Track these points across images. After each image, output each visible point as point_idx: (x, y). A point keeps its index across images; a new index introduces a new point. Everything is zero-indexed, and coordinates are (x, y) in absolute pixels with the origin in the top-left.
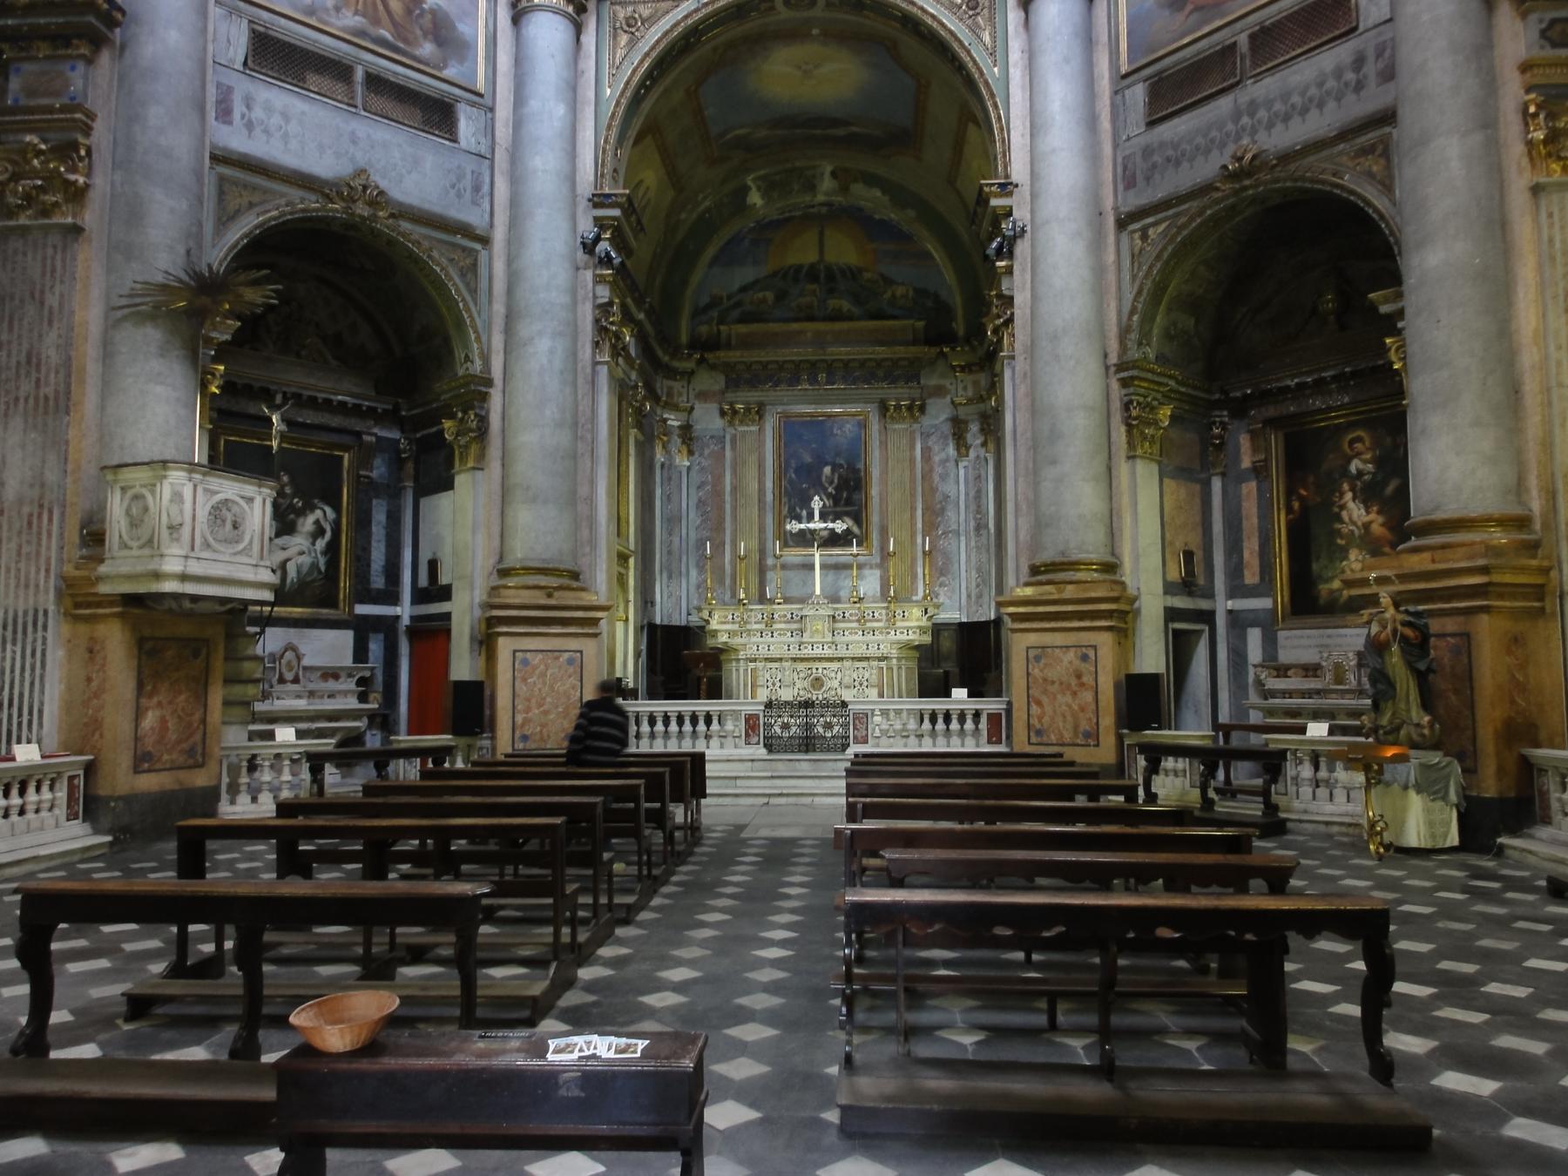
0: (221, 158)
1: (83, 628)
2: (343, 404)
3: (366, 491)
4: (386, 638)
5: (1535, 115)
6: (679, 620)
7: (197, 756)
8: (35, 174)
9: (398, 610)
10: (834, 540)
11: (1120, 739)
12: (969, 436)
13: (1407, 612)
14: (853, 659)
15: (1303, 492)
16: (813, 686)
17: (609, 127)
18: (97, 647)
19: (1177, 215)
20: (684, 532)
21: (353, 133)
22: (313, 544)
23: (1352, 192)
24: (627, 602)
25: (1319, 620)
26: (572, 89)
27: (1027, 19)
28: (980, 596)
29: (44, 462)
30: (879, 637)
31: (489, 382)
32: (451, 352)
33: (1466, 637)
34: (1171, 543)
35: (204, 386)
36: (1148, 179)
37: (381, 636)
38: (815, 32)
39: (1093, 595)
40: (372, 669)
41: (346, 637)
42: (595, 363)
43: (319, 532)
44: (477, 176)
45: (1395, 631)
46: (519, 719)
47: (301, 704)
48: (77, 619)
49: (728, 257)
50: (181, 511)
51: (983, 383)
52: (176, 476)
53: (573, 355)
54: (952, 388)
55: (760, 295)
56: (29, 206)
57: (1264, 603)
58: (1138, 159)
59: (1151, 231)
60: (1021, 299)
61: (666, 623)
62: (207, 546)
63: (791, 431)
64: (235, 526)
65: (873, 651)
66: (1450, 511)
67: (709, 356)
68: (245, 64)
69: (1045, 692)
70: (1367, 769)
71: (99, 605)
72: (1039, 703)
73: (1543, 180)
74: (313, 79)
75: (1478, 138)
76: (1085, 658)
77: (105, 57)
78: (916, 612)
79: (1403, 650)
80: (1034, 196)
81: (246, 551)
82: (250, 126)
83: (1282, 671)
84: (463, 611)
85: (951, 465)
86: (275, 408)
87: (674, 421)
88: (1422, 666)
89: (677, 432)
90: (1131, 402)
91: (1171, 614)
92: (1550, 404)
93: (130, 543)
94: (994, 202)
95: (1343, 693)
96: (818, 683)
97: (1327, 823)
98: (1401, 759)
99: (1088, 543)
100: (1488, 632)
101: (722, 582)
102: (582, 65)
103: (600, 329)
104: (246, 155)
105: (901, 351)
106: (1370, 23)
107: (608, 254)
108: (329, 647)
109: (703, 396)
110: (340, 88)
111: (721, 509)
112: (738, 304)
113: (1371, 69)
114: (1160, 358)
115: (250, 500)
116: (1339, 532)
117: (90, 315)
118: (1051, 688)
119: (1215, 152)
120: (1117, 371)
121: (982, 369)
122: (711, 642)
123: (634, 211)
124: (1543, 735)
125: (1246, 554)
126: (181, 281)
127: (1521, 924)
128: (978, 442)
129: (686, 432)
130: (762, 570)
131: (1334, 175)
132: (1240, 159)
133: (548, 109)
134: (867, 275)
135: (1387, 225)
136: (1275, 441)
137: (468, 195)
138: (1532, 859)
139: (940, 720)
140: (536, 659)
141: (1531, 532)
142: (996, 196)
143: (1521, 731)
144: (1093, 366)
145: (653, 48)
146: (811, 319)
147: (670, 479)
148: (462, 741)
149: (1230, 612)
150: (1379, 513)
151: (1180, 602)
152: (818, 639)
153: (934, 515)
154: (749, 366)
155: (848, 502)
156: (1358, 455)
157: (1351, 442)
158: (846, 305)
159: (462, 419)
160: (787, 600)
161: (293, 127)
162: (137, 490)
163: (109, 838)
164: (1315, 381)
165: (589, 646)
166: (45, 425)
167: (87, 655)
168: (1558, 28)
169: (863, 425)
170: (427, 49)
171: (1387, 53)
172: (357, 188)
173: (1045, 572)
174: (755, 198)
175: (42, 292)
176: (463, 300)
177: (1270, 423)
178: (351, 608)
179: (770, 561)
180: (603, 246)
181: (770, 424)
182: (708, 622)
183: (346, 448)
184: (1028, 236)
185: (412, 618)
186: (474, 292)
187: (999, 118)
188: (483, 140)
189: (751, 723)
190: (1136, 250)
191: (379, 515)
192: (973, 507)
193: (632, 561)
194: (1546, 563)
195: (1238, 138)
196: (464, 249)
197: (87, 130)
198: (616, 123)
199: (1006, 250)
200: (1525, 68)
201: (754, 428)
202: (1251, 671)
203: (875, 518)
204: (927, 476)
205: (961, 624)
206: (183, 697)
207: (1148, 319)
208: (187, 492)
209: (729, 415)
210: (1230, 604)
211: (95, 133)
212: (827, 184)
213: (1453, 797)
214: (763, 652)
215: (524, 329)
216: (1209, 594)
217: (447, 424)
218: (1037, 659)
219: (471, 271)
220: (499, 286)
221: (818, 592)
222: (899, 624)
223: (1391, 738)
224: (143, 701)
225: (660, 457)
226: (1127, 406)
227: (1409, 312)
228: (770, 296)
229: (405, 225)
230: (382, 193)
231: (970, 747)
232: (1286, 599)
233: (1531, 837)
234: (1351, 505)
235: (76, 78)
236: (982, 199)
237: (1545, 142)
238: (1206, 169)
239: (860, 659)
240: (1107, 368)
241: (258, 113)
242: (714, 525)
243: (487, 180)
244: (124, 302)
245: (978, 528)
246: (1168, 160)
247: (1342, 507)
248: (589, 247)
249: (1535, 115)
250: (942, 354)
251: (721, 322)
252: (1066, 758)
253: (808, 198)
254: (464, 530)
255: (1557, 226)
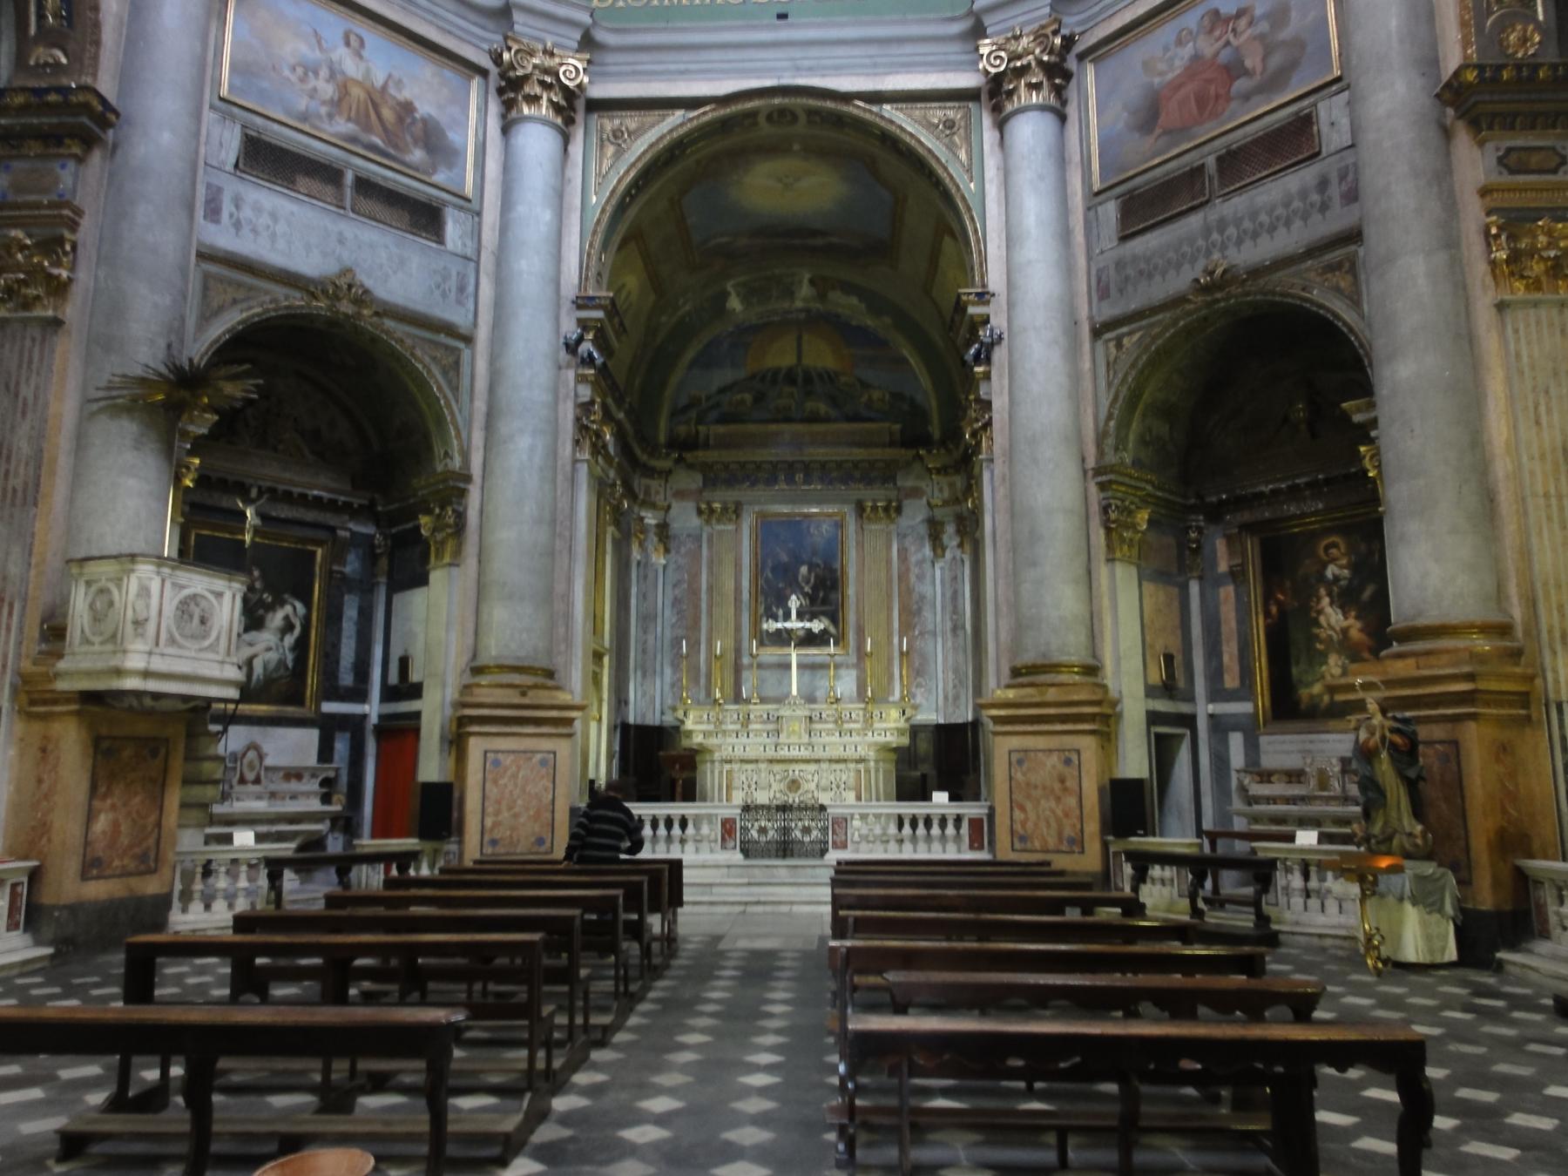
0: (207, 255)
1: (37, 727)
2: (318, 499)
3: (338, 586)
4: (353, 738)
5: (1497, 236)
6: (653, 719)
7: (149, 862)
8: (18, 268)
9: (366, 708)
10: (810, 639)
11: (1105, 846)
12: (945, 538)
13: (1394, 718)
14: (830, 761)
15: (1280, 597)
16: (790, 789)
17: (595, 232)
18: (50, 747)
19: (1152, 325)
20: (659, 629)
21: (340, 233)
22: (282, 640)
23: (1321, 306)
24: (600, 701)
25: (1303, 725)
26: (559, 196)
27: (1002, 137)
28: (956, 698)
29: (7, 554)
30: (855, 738)
31: (468, 479)
32: (430, 448)
33: (1455, 743)
34: (1152, 647)
35: (178, 479)
36: (1121, 291)
37: (348, 735)
38: (796, 147)
39: (1076, 698)
40: (337, 770)
41: (311, 736)
42: (575, 461)
43: (288, 627)
44: (462, 278)
45: (1383, 738)
46: (489, 822)
47: (261, 806)
48: (31, 716)
49: (706, 361)
50: (148, 606)
51: (959, 485)
52: (145, 570)
53: (553, 453)
54: (929, 490)
55: (739, 397)
56: (10, 298)
57: (1243, 708)
58: (1112, 272)
59: (1125, 341)
60: (999, 404)
61: (639, 722)
62: (172, 641)
63: (767, 529)
64: (203, 621)
65: (850, 753)
66: (1431, 618)
67: (688, 456)
68: (236, 166)
69: (1029, 797)
70: (1361, 879)
71: (55, 702)
72: (1022, 808)
73: (1508, 297)
74: (303, 182)
75: (1441, 258)
76: (1068, 762)
77: (96, 157)
78: (894, 713)
79: (1391, 755)
80: (1011, 305)
81: (212, 648)
82: (237, 225)
83: (1266, 776)
84: (433, 710)
85: (928, 565)
86: (248, 501)
87: (651, 519)
88: (1412, 773)
89: (654, 530)
90: (1109, 505)
91: (1153, 718)
92: (1526, 513)
93: (92, 638)
94: (972, 310)
95: (1328, 800)
96: (794, 785)
97: (1320, 936)
98: (1395, 870)
99: (1069, 646)
100: (1476, 740)
101: (696, 681)
102: (569, 173)
103: (581, 427)
104: (232, 253)
105: (877, 453)
106: (1332, 148)
107: (590, 354)
108: (293, 746)
109: (680, 495)
110: (329, 190)
111: (697, 607)
112: (718, 405)
113: (1335, 191)
114: (1137, 463)
115: (219, 595)
116: (1317, 637)
117: (65, 406)
118: (1034, 793)
119: (1187, 266)
120: (1095, 476)
121: (957, 471)
122: (685, 743)
123: (617, 313)
124: (1536, 845)
125: (1226, 658)
126: (160, 375)
127: (1533, 1047)
128: (954, 543)
129: (663, 530)
130: (738, 670)
131: (1304, 289)
132: (1211, 273)
133: (534, 214)
134: (843, 379)
135: (1357, 337)
136: (1251, 546)
137: (453, 295)
138: (1533, 976)
139: (921, 825)
140: (507, 760)
141: (1514, 639)
142: (974, 304)
143: (1513, 841)
144: (1071, 470)
145: (639, 158)
146: (788, 420)
147: (645, 577)
148: (428, 846)
149: (1211, 716)
150: (1357, 618)
151: (1162, 706)
152: (794, 741)
153: (911, 616)
154: (726, 466)
155: (825, 602)
156: (1333, 560)
157: (1327, 548)
158: (823, 408)
159: (439, 516)
160: (763, 700)
161: (281, 228)
162: (103, 583)
163: (49, 951)
164: (1289, 487)
165: (563, 747)
166: (12, 516)
167: (40, 755)
168: (1553, 165)
169: (840, 525)
170: (417, 155)
171: (1350, 177)
172: (343, 287)
173: (1027, 674)
174: (735, 303)
175: (18, 384)
176: (445, 397)
177: (1247, 528)
178: (318, 707)
179: (746, 660)
180: (586, 347)
181: (747, 523)
182: (682, 722)
183: (319, 543)
184: (1005, 343)
185: (381, 717)
186: (455, 389)
187: (976, 230)
188: (469, 243)
189: (728, 827)
190: (1112, 359)
191: (350, 612)
192: (949, 608)
193: (606, 660)
194: (1530, 671)
195: (1208, 253)
196: (447, 347)
197: (73, 226)
198: (602, 228)
199: (984, 356)
200: (1484, 192)
201: (731, 527)
202: (1234, 776)
203: (851, 617)
204: (903, 577)
205: (939, 727)
206: (137, 800)
207: (1124, 424)
208: (155, 586)
209: (707, 514)
210: (1211, 708)
211: (82, 230)
212: (805, 290)
213: (1449, 908)
214: (739, 752)
215: (504, 427)
216: (1190, 698)
217: (424, 520)
218: (1020, 762)
219: (453, 368)
220: (481, 384)
221: (794, 692)
222: (876, 725)
223: (1383, 848)
224: (97, 803)
225: (636, 554)
226: (1105, 510)
227: (1382, 422)
228: (748, 397)
229: (389, 323)
230: (366, 291)
231: (951, 854)
232: (1267, 704)
233: (1530, 952)
234: (1329, 610)
235: (66, 176)
236: (960, 307)
237: (1508, 262)
238: (1179, 282)
239: (838, 761)
240: (1085, 472)
241: (246, 213)
242: (689, 623)
243: (472, 281)
244: (101, 394)
245: (955, 629)
246: (1141, 273)
247: (1320, 612)
248: (571, 347)
249: (1497, 236)
250: (920, 458)
251: (700, 421)
252: (1054, 867)
253: (786, 305)
254: (437, 627)
255: (1523, 341)
